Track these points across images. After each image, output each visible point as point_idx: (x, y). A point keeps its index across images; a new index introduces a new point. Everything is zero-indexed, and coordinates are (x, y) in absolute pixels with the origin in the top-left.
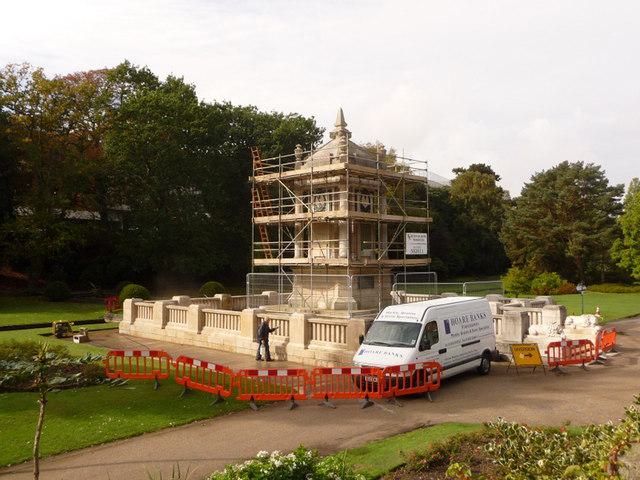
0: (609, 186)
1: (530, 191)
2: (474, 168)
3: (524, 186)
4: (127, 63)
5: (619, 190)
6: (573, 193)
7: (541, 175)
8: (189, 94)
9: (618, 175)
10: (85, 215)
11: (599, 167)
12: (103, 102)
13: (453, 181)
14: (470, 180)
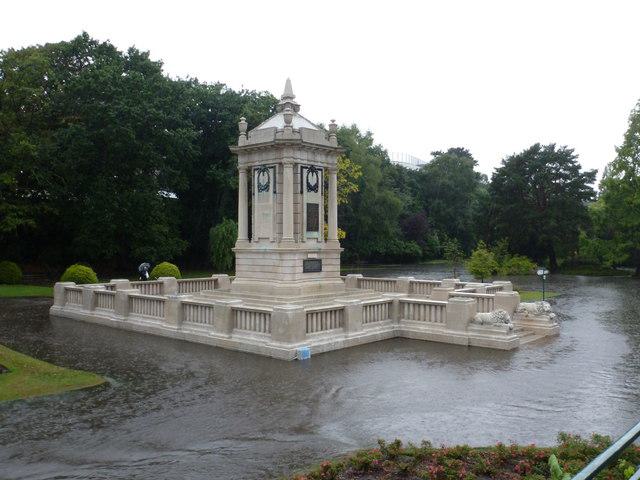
1: (500, 176)
2: (452, 151)
3: (495, 171)
4: (85, 35)
5: (591, 176)
6: (539, 177)
7: (512, 159)
8: (153, 70)
9: (597, 156)
11: (573, 150)
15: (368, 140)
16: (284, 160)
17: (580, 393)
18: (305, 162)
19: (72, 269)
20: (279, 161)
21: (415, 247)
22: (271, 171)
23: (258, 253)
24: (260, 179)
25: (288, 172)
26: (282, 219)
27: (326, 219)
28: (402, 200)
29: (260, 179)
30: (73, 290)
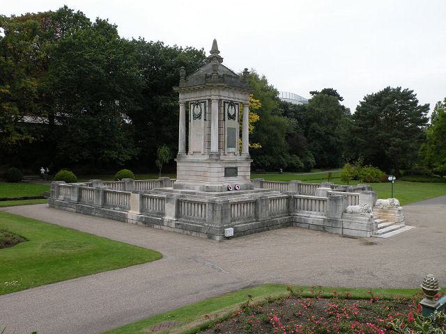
0: (418, 105)
5: (426, 108)
6: (392, 107)
7: (370, 97)
9: (428, 97)
10: (39, 120)
12: (50, 36)
13: (310, 101)
14: (321, 99)
15: (264, 81)
16: (213, 97)
17: (82, 207)
18: (227, 98)
19: (62, 172)
20: (208, 98)
21: (296, 160)
22: (203, 104)
23: (193, 162)
24: (195, 110)
25: (215, 106)
26: (210, 139)
27: (241, 136)
28: (289, 123)
29: (195, 110)
30: (64, 187)
